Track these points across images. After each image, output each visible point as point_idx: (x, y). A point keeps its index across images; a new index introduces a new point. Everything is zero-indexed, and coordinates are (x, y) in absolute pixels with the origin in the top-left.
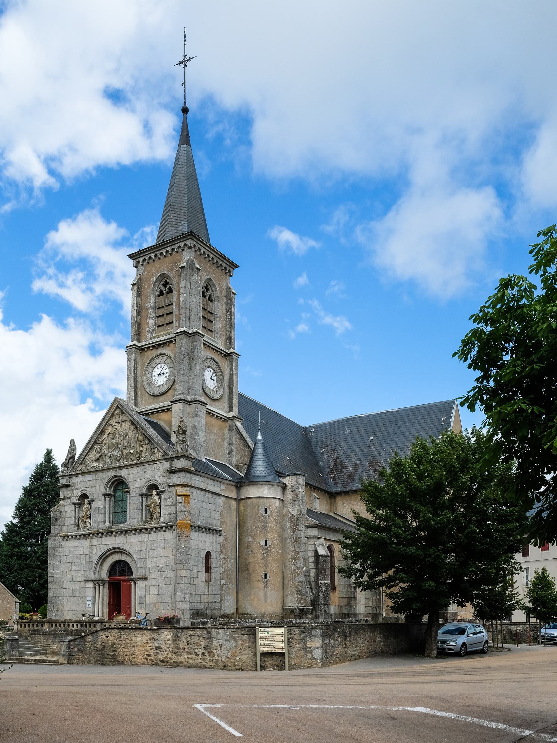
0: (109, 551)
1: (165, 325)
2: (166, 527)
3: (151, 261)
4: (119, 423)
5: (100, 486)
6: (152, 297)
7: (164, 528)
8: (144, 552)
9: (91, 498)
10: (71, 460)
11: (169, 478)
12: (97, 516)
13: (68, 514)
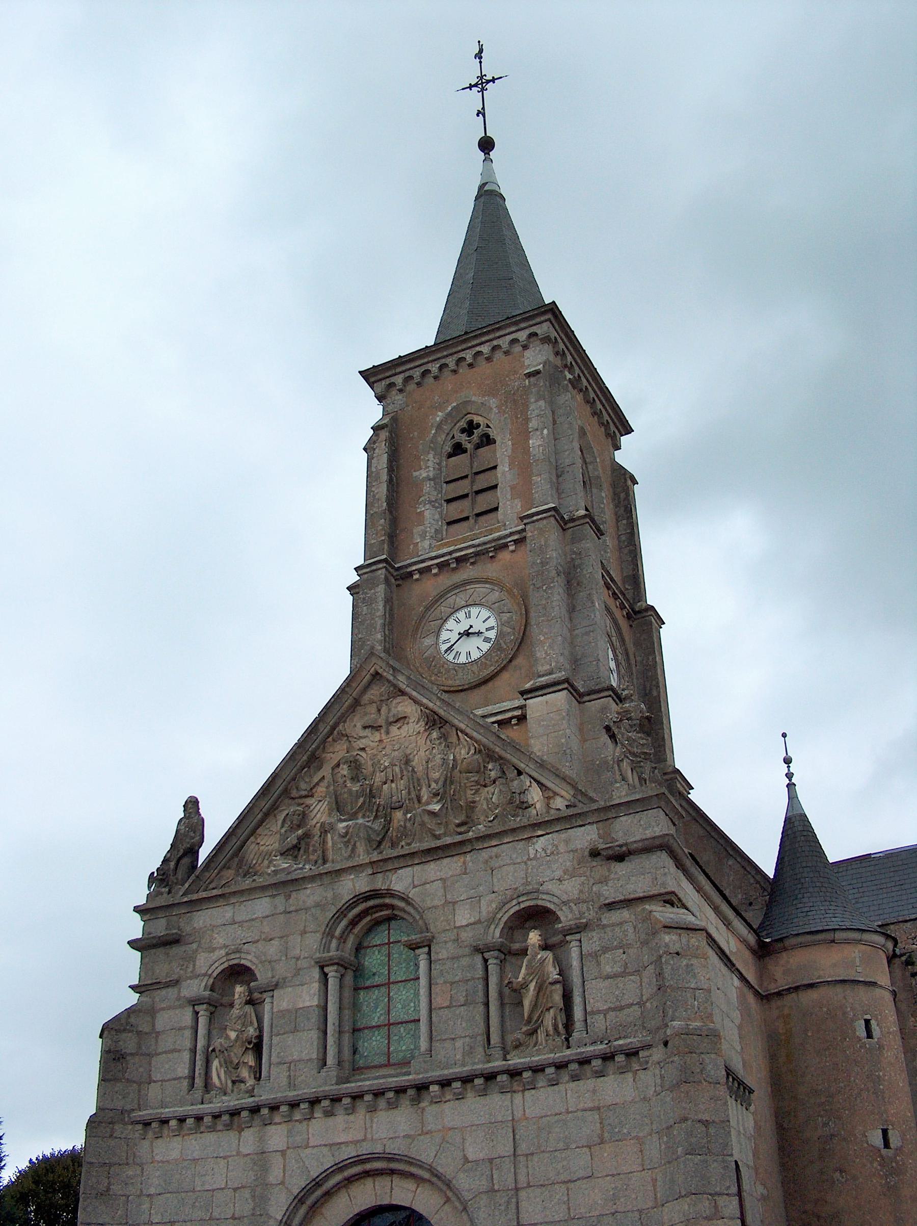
0: (341, 1169)
1: (472, 520)
2: (608, 1058)
3: (429, 380)
4: (377, 728)
5: (304, 933)
6: (431, 456)
7: (597, 1063)
8: (508, 1165)
9: (263, 976)
10: (186, 861)
11: (604, 881)
12: (290, 1039)
13: (166, 1042)
